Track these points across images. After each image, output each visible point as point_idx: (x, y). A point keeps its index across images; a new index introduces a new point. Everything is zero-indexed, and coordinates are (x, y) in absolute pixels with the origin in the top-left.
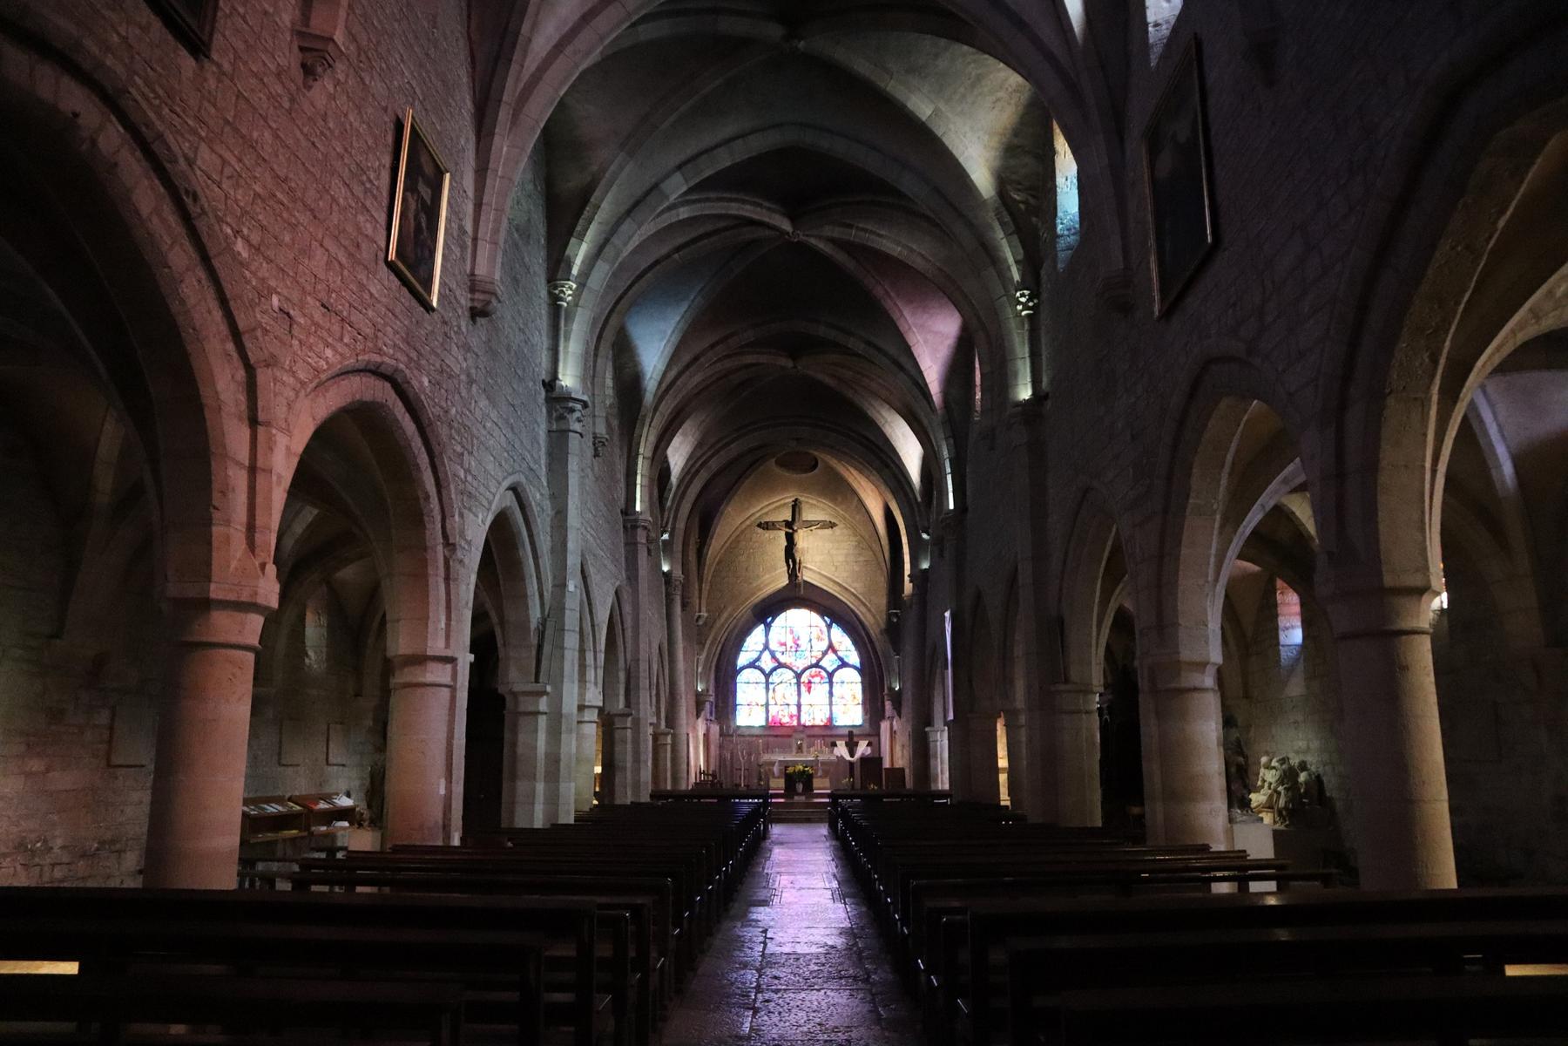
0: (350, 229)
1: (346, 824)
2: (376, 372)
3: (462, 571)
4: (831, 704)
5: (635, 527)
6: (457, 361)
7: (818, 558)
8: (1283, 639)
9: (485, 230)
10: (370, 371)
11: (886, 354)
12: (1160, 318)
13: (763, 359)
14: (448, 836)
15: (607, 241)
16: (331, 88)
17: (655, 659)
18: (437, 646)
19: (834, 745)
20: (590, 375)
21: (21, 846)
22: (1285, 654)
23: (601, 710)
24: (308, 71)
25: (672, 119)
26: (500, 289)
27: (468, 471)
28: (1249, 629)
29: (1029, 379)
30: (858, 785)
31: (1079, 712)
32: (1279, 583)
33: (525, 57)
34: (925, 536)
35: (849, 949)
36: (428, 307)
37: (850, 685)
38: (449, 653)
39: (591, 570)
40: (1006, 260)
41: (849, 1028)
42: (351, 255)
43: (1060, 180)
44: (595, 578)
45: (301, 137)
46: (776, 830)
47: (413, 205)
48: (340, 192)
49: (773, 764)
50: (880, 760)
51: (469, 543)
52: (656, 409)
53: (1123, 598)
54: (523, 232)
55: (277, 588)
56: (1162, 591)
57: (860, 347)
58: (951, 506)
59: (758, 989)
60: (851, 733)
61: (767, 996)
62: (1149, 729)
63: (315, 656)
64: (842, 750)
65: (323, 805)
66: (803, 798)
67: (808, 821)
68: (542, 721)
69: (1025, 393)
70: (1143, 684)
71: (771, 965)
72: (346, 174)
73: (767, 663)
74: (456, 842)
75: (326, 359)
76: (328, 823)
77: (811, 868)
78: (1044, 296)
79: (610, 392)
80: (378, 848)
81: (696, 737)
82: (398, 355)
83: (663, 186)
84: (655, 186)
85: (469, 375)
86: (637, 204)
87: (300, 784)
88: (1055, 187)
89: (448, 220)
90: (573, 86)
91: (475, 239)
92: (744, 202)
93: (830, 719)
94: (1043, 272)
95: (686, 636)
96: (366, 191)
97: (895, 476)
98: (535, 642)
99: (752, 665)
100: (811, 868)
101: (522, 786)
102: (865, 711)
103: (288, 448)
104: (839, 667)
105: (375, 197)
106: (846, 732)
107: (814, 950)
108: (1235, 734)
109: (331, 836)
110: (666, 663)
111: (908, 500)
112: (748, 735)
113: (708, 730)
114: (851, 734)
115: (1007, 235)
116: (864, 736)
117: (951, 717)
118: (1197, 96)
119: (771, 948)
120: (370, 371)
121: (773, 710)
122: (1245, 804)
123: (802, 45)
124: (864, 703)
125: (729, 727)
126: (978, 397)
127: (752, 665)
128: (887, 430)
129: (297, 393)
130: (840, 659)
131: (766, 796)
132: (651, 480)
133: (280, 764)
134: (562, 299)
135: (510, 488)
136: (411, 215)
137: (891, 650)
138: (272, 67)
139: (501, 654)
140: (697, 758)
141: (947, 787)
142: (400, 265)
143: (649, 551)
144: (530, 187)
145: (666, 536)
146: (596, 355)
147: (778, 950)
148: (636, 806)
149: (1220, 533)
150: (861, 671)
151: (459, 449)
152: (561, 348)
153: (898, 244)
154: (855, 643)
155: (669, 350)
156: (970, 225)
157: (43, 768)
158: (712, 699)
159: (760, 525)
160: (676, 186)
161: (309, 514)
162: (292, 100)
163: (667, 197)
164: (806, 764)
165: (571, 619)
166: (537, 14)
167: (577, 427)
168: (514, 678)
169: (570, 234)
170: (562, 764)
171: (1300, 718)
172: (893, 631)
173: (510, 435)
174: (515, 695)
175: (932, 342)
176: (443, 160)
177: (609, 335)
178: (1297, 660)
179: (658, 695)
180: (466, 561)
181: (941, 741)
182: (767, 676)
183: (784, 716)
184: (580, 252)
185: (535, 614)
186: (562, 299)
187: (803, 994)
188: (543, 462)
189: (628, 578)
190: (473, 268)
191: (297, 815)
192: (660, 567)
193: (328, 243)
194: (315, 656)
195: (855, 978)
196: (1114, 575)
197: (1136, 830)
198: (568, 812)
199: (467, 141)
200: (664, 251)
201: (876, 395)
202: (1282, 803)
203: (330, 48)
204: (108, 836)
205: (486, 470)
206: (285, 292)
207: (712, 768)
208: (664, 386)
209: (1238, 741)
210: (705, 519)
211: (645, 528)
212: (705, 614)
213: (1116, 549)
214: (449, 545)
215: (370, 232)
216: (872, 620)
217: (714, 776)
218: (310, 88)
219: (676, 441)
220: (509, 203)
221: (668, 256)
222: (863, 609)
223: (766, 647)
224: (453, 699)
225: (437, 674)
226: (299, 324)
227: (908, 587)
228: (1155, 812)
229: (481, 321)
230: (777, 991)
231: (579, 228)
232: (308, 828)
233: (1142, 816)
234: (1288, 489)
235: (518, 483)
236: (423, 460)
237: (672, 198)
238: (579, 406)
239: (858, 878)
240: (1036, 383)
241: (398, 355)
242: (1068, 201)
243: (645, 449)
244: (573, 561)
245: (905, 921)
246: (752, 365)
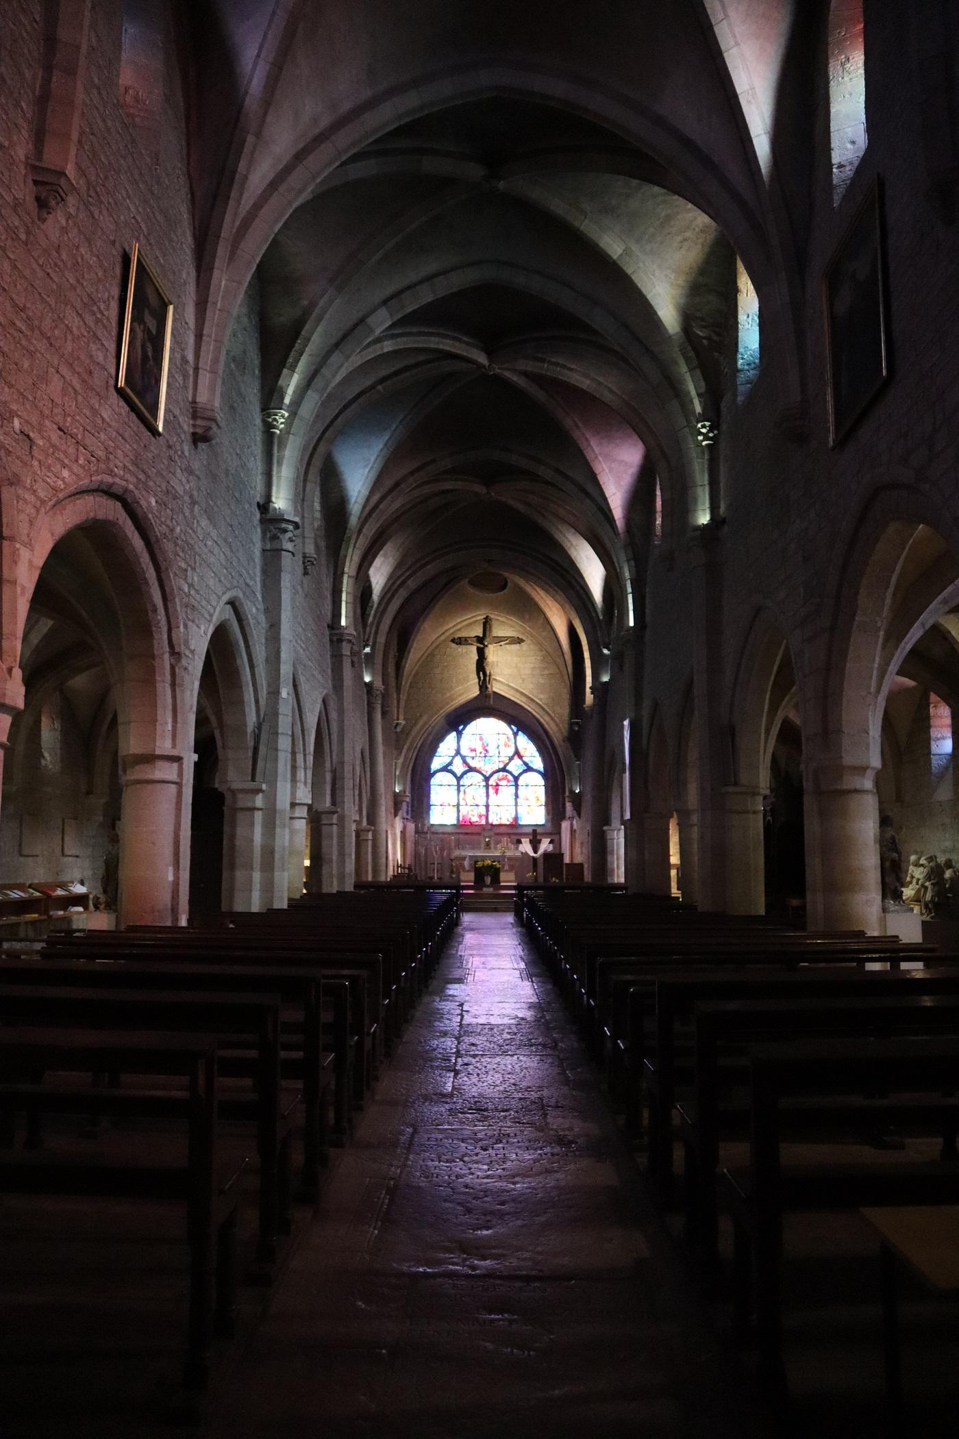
0: (83, 357)
1: (81, 909)
2: (107, 492)
3: (187, 678)
4: (516, 805)
5: (340, 641)
6: (180, 483)
7: (507, 671)
8: (935, 748)
9: (206, 362)
10: (103, 491)
11: (574, 482)
12: (833, 448)
13: (459, 485)
14: (176, 918)
16: (64, 222)
17: (358, 762)
18: (164, 746)
19: (519, 842)
20: (300, 498)
22: (935, 762)
23: (310, 807)
24: (42, 204)
25: (380, 253)
26: (220, 417)
27: (191, 586)
28: (906, 737)
29: (707, 505)
30: (541, 880)
31: (748, 812)
32: (933, 697)
33: (241, 194)
34: (606, 651)
35: (537, 1020)
36: (154, 432)
37: (534, 790)
38: (175, 753)
39: (302, 679)
40: (689, 393)
41: (540, 1088)
42: (84, 381)
43: (742, 317)
44: (304, 687)
45: (38, 269)
46: (467, 918)
47: (140, 335)
48: (73, 321)
49: (464, 858)
50: (561, 855)
51: (193, 652)
52: (360, 531)
53: (788, 711)
54: (239, 362)
55: (22, 690)
56: (828, 701)
57: (548, 474)
58: (632, 624)
59: (458, 1054)
60: (534, 831)
61: (466, 1060)
62: (812, 826)
63: (50, 759)
64: (526, 847)
65: (60, 892)
66: (491, 890)
67: (496, 910)
68: (258, 816)
69: (704, 518)
70: (808, 785)
71: (467, 1033)
72: (78, 305)
73: (458, 767)
74: (183, 922)
75: (63, 479)
76: (65, 909)
77: (500, 951)
78: (724, 427)
79: (318, 515)
80: (113, 928)
81: (394, 834)
82: (128, 476)
84: (362, 320)
85: (191, 497)
86: (344, 337)
87: (38, 873)
88: (737, 323)
89: (172, 350)
90: (286, 224)
91: (196, 369)
92: (446, 337)
93: (516, 819)
94: (723, 405)
95: (385, 741)
96: (97, 321)
97: (580, 597)
98: (251, 744)
99: (445, 769)
100: (500, 951)
101: (240, 875)
102: (548, 812)
103: (30, 561)
104: (525, 771)
105: (105, 327)
106: (530, 830)
107: (506, 1021)
108: (890, 832)
109: (68, 920)
110: (368, 769)
111: (591, 618)
112: (440, 833)
113: (405, 828)
114: (535, 833)
115: (691, 370)
116: (546, 835)
117: (628, 816)
118: (878, 232)
119: (468, 1019)
120: (103, 491)
121: (463, 810)
122: (897, 896)
123: (501, 185)
124: (547, 805)
125: (423, 825)
126: (659, 521)
127: (445, 769)
128: (573, 553)
129: (38, 510)
130: (525, 764)
131: (459, 888)
132: (355, 597)
133: (21, 855)
134: (275, 427)
135: (228, 603)
136: (138, 344)
137: (573, 755)
138: (9, 199)
139: (220, 751)
140: (395, 854)
141: (622, 880)
142: (128, 391)
143: (353, 662)
144: (245, 320)
145: (368, 650)
146: (305, 481)
147: (474, 1021)
148: (341, 894)
149: (884, 648)
150: (545, 775)
151: (183, 565)
152: (274, 473)
153: (586, 376)
154: (539, 750)
155: (373, 476)
156: (654, 358)
158: (408, 799)
159: (453, 641)
160: (381, 321)
161: (46, 625)
162: (28, 233)
163: (372, 331)
164: (494, 859)
165: (285, 722)
166: (252, 153)
167: (289, 546)
168: (233, 777)
169: (282, 364)
170: (277, 856)
171: (947, 821)
172: (575, 739)
173: (228, 553)
174: (233, 792)
175: (616, 471)
176: (168, 295)
177: (318, 462)
178: (946, 768)
179: (360, 795)
180: (190, 668)
181: (618, 839)
182: (459, 779)
183: (474, 815)
184: (291, 384)
185: (251, 719)
187: (498, 1059)
188: (258, 579)
189: (334, 687)
190: (194, 396)
191: (37, 900)
193: (64, 370)
194: (50, 759)
195: (544, 1046)
196: (782, 688)
197: (799, 919)
198: (281, 898)
199: (188, 274)
200: (368, 383)
201: (564, 521)
202: (928, 897)
203: (63, 181)
205: (207, 586)
206: (24, 414)
207: (408, 863)
208: (368, 508)
209: (893, 838)
210: (403, 635)
211: (350, 641)
212: (402, 722)
213: (786, 665)
214: (175, 654)
215: (100, 358)
216: (555, 728)
217: (409, 869)
218: (44, 220)
219: (378, 562)
220: (229, 332)
221: (373, 387)
222: (547, 718)
223: (458, 752)
224: (180, 794)
225: (167, 771)
226: (38, 446)
227: (589, 698)
228: (815, 902)
229: (202, 446)
230: (474, 1056)
231: (290, 360)
232: (46, 912)
233: (803, 908)
234: (947, 609)
235: (236, 597)
236: (151, 574)
237: (378, 332)
238: (291, 527)
239: (543, 959)
240: (714, 509)
241: (128, 476)
242: (749, 337)
243: (350, 568)
244: (286, 669)
245: (590, 994)
246: (448, 491)
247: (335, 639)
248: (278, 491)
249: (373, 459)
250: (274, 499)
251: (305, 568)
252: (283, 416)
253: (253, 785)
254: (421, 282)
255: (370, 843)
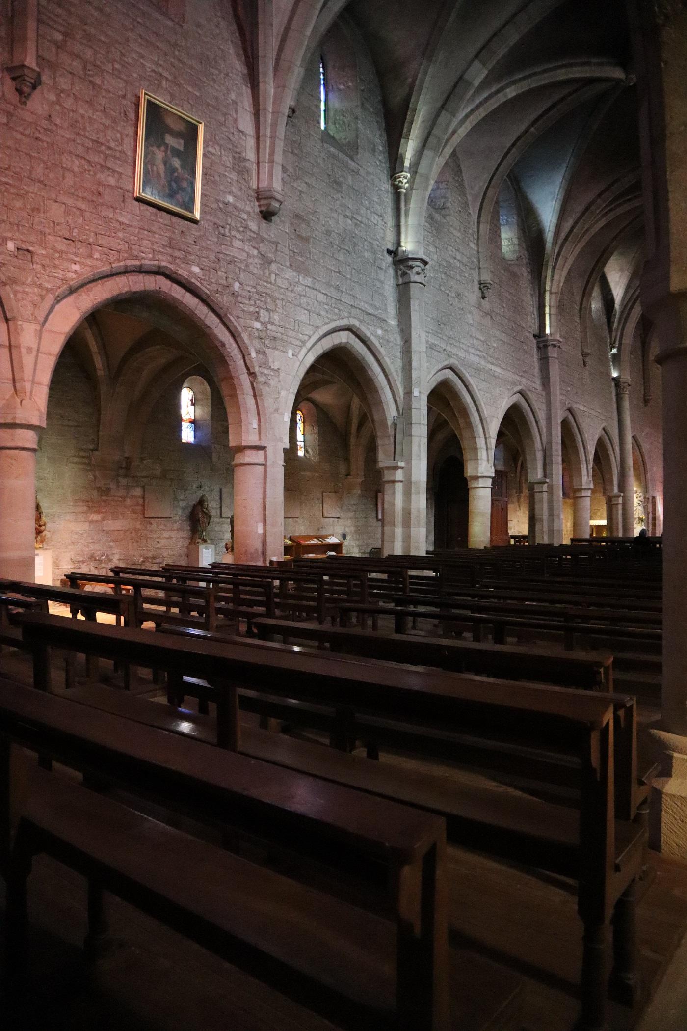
5: (546, 346)
15: (429, 134)
16: (52, 97)
21: (92, 557)
68: (399, 487)
83: (466, 77)
84: (461, 78)
92: (571, 65)
134: (400, 187)
145: (614, 351)
155: (558, 207)
157: (99, 518)
160: (478, 74)
169: (400, 137)
185: (391, 412)
186: (400, 187)
192: (609, 374)
204: (150, 554)
218: (25, 103)
221: (526, 131)
231: (405, 130)
237: (476, 83)
238: (418, 263)
247: (541, 345)
248: (406, 237)
249: (557, 191)
250: (402, 244)
251: (483, 293)
252: (406, 178)
253: (392, 464)
254: (504, 26)
255: (620, 507)
